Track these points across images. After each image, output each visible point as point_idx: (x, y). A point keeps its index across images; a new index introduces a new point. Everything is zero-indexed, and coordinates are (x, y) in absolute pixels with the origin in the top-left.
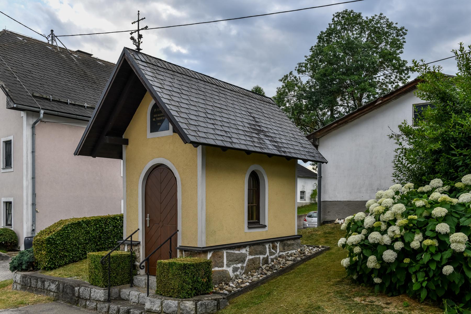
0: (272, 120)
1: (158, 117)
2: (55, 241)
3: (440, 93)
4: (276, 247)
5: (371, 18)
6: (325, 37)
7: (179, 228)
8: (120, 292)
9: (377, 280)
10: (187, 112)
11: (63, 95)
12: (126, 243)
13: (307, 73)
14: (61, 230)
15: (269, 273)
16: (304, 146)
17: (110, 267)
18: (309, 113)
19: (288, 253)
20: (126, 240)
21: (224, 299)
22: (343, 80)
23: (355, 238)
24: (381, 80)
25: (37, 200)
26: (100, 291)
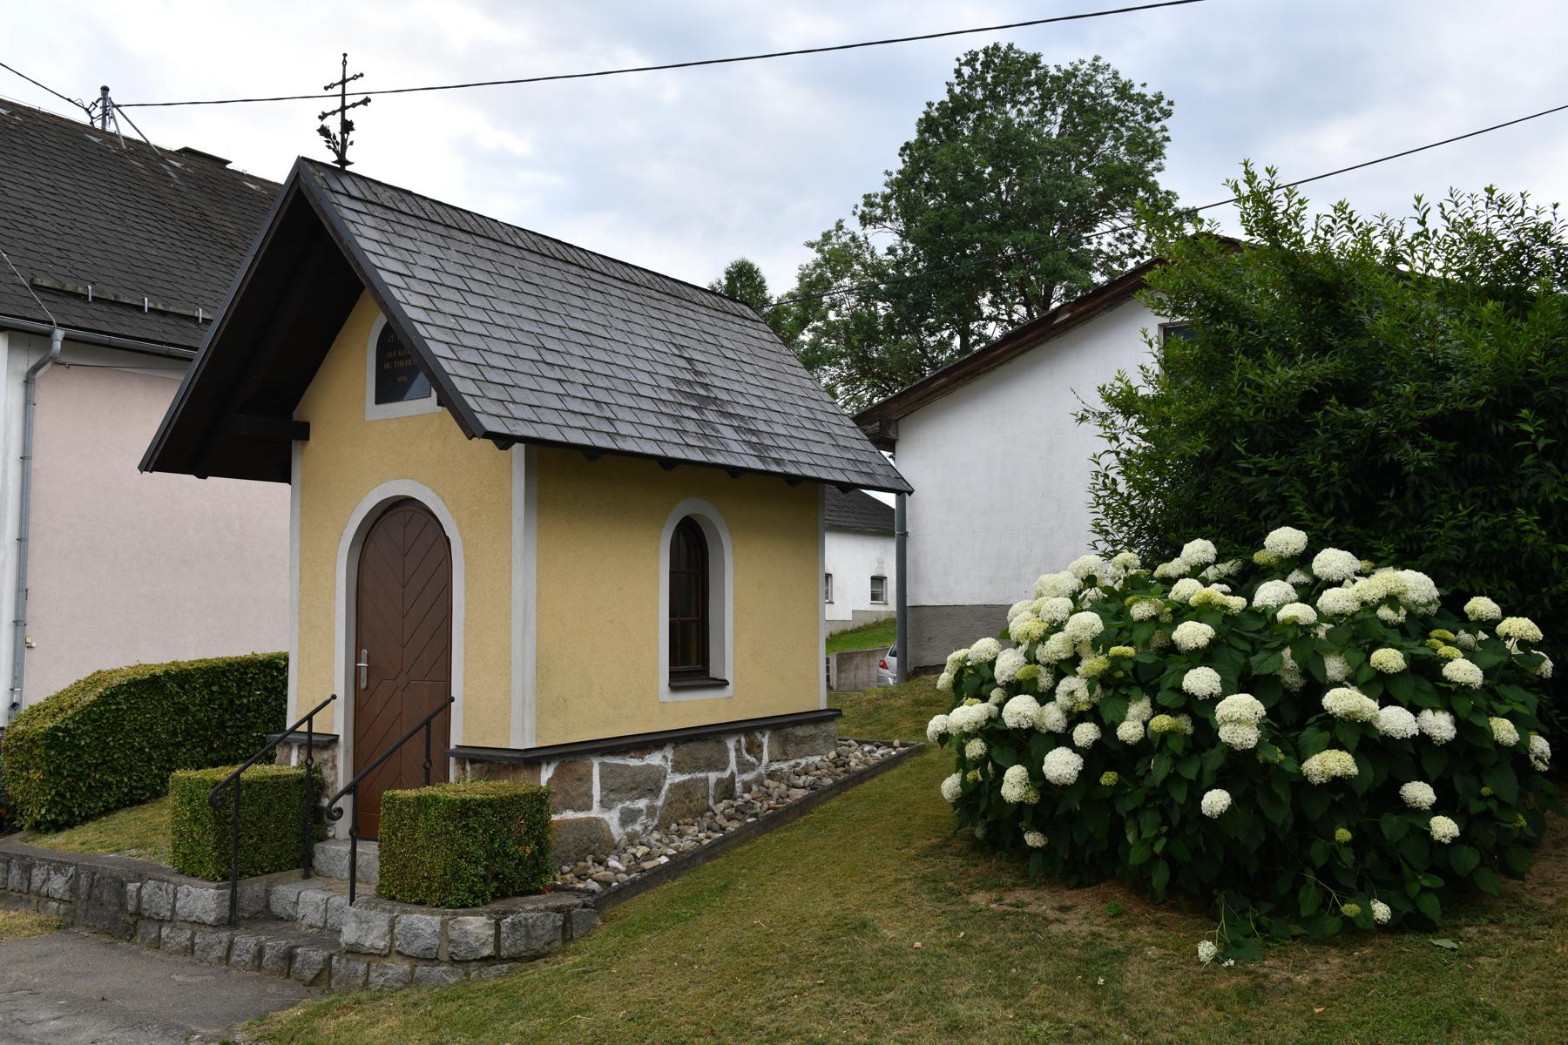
0: (748, 369)
1: (399, 359)
2: (73, 737)
3: (1206, 298)
4: (760, 746)
5: (1070, 68)
7: (456, 691)
8: (268, 893)
9: (1033, 839)
10: (481, 345)
11: (127, 284)
12: (295, 741)
13: (888, 224)
14: (94, 704)
15: (732, 826)
16: (842, 442)
17: (238, 815)
18: (896, 342)
19: (798, 764)
20: (293, 730)
21: (585, 906)
22: (994, 244)
23: (969, 713)
24: (1104, 248)
25: (33, 609)
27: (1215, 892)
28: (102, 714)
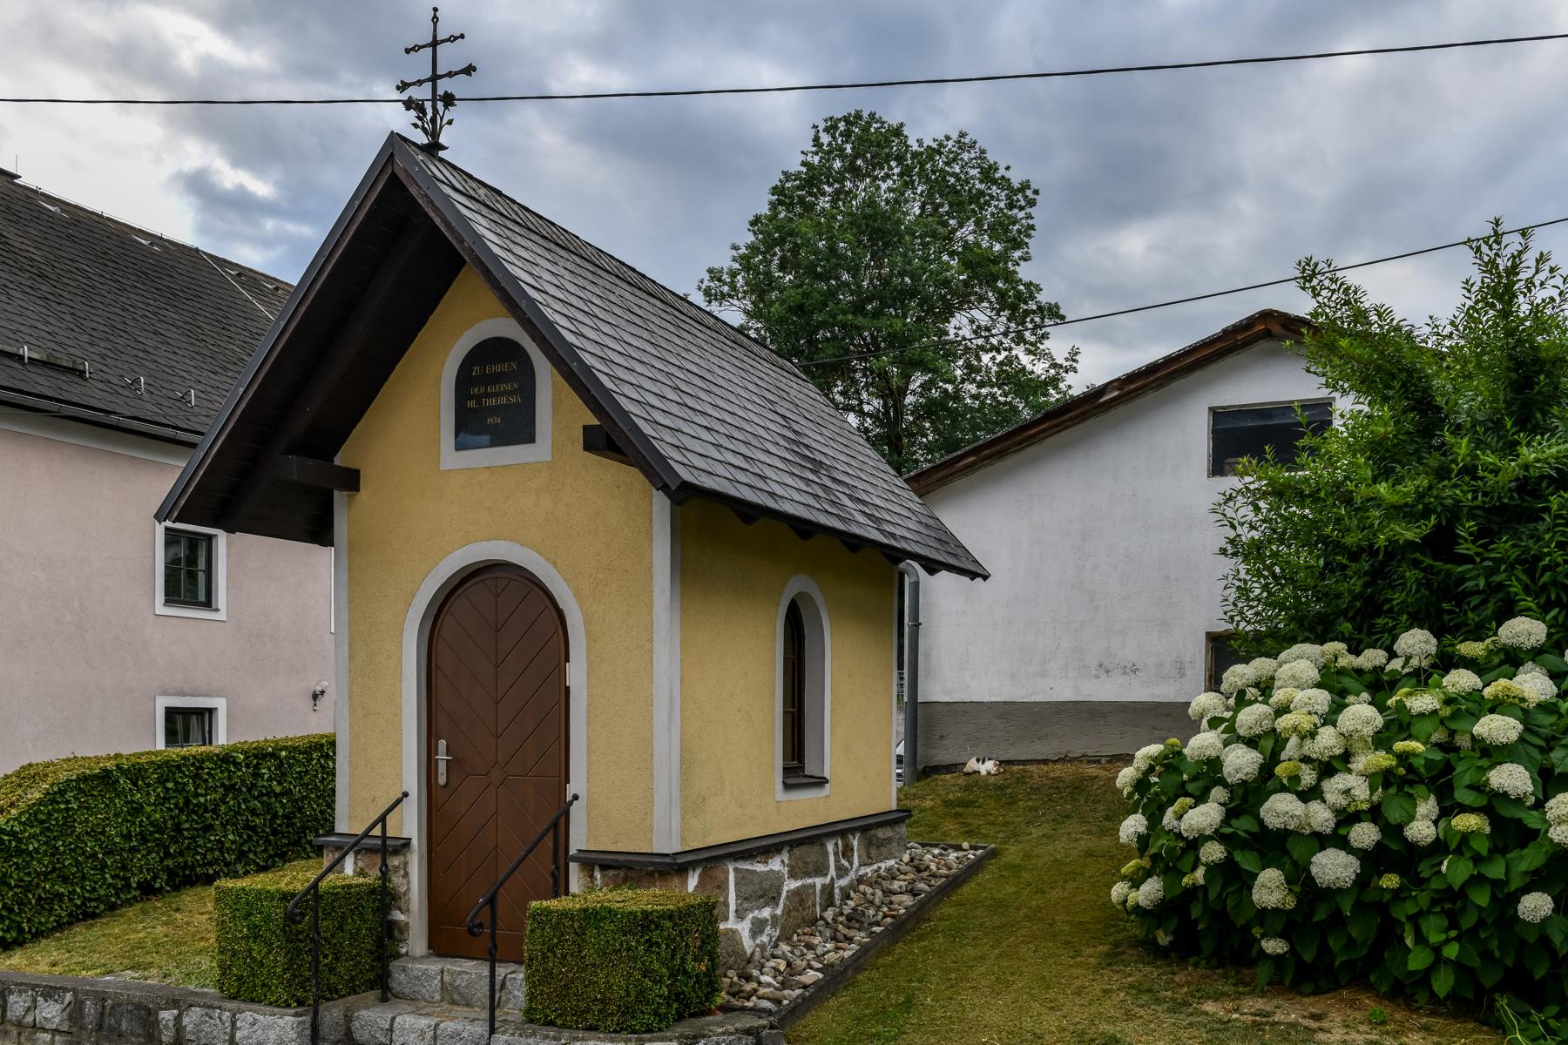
1: (488, 395)
5: (935, 145)
6: (795, 194)
8: (348, 1019)
14: (40, 802)
21: (772, 1027)
26: (281, 1022)
27: (1497, 996)
28: (50, 814)
